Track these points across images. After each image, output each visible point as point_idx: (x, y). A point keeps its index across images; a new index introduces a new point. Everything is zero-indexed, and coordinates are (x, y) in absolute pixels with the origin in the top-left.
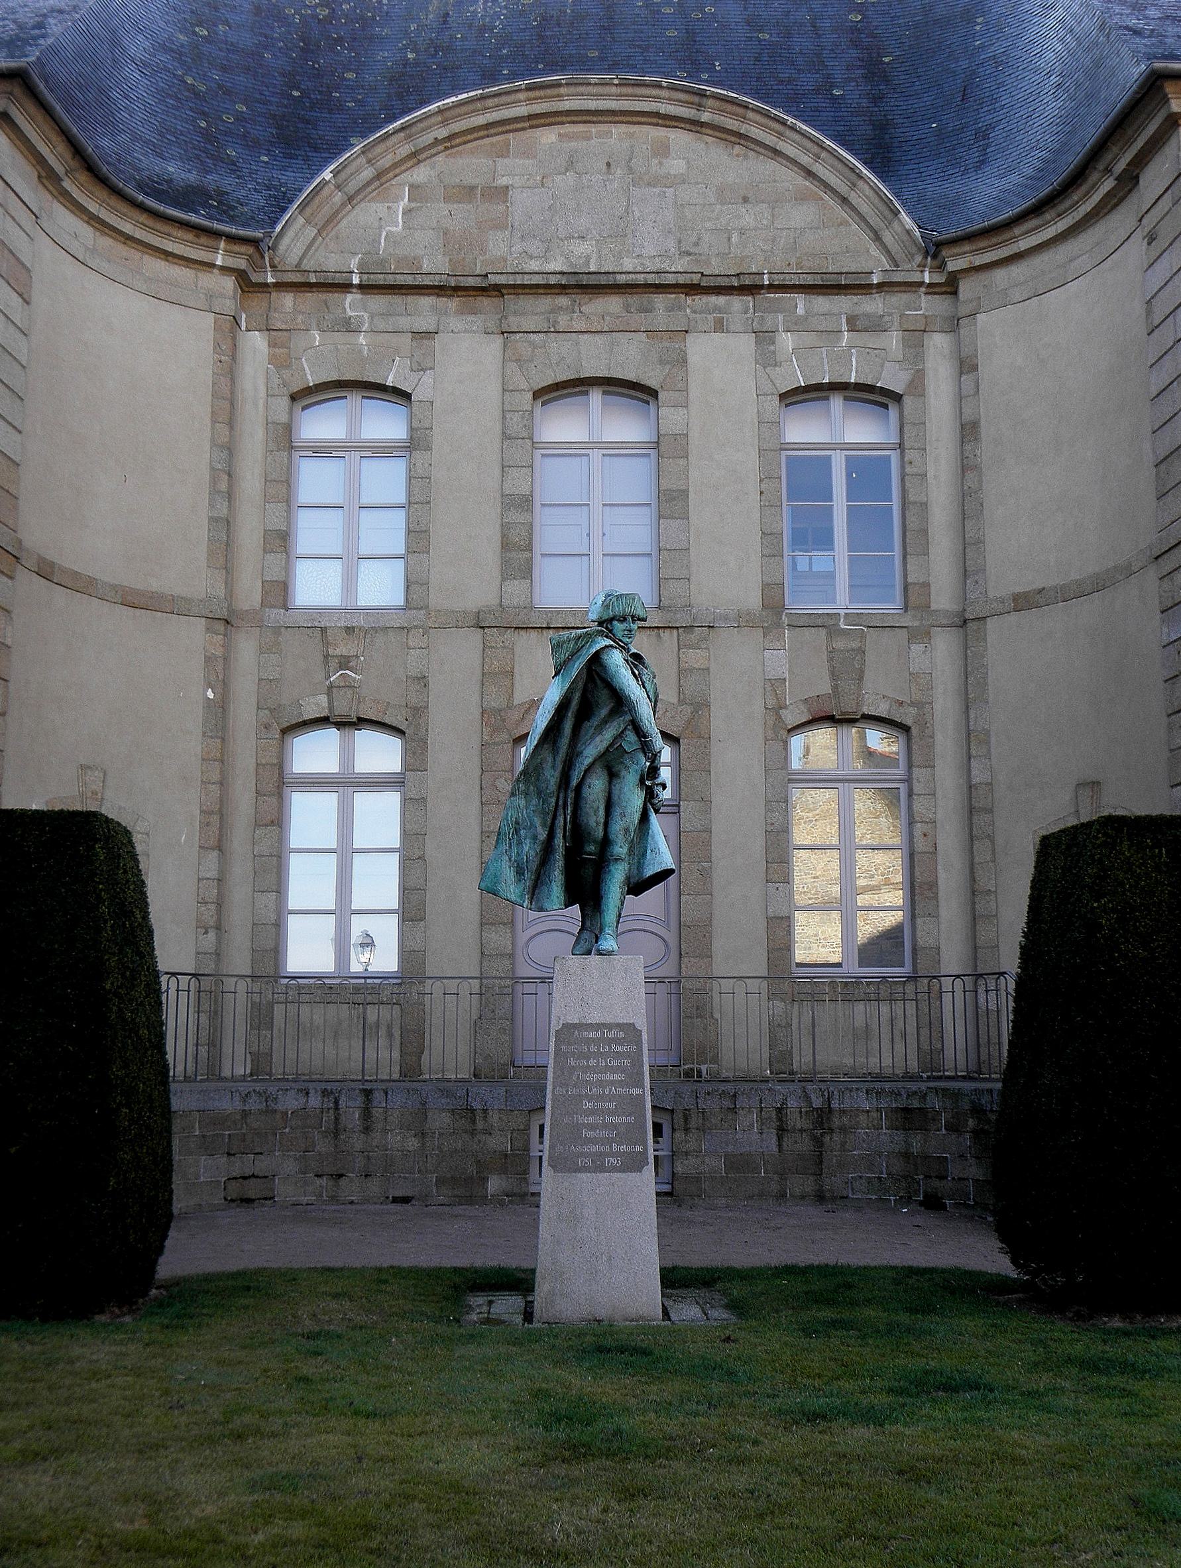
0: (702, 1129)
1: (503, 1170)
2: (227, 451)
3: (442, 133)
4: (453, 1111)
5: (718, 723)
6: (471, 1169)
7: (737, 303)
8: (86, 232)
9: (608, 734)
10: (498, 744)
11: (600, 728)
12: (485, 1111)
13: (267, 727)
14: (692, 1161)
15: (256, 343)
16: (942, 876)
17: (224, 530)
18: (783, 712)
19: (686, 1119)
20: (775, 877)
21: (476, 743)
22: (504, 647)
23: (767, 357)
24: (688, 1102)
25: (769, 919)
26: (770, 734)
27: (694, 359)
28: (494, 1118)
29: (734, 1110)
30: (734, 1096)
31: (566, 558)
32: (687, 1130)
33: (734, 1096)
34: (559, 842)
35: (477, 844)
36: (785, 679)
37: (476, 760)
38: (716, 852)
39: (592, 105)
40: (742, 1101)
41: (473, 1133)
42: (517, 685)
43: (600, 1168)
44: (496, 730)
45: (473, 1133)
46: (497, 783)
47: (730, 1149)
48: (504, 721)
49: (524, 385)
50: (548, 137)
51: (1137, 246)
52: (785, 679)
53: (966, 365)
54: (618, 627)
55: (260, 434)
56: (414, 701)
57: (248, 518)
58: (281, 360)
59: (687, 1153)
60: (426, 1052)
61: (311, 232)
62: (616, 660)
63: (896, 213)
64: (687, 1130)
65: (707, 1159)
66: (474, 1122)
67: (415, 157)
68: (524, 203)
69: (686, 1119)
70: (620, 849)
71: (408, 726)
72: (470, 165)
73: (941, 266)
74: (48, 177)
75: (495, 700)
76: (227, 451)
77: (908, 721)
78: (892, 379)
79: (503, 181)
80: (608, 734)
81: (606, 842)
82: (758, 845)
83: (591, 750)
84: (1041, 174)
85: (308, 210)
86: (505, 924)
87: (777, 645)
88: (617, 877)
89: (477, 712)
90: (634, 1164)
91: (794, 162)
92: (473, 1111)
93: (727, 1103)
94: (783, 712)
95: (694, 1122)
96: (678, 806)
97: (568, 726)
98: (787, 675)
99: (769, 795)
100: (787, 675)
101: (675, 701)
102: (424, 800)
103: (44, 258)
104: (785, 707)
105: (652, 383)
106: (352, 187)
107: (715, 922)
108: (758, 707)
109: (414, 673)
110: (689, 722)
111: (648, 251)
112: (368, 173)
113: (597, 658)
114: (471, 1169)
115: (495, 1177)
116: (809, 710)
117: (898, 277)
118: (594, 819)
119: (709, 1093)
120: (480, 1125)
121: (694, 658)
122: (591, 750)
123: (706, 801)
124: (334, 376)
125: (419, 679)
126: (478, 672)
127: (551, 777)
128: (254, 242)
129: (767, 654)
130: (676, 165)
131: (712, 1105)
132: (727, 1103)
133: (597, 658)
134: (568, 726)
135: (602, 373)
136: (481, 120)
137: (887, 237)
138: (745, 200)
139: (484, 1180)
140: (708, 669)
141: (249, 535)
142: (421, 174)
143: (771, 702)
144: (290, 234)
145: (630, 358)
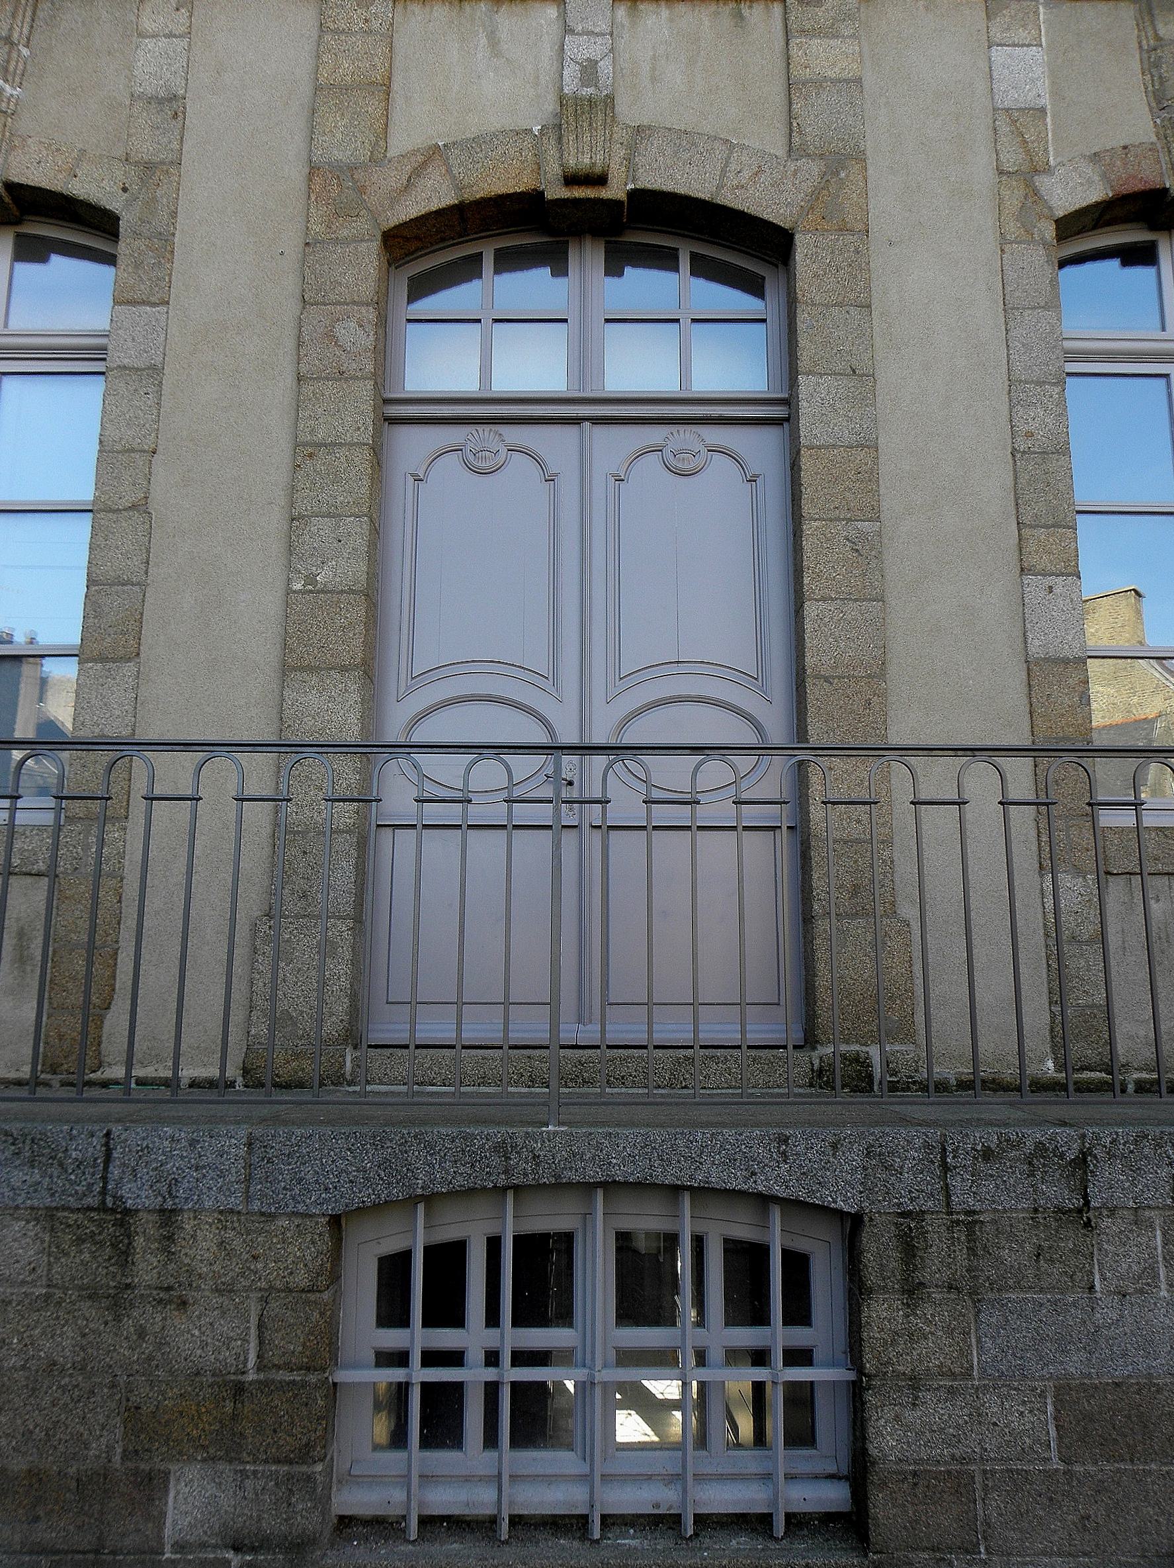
0: (969, 1290)
1: (225, 1446)
4: (49, 1217)
5: (885, 199)
6: (106, 1443)
10: (345, 242)
12: (168, 1216)
14: (935, 1410)
18: (1044, 183)
19: (909, 1248)
20: (1044, 562)
21: (291, 241)
22: (369, 32)
24: (912, 1184)
25: (1029, 664)
26: (1013, 228)
28: (201, 1244)
29: (1082, 1216)
30: (1082, 1161)
31: (578, 674)
32: (912, 1291)
33: (1082, 1161)
35: (280, 476)
36: (1043, 110)
37: (291, 283)
38: (890, 502)
40: (1108, 1184)
41: (117, 1301)
42: (397, 116)
44: (342, 212)
45: (117, 1301)
46: (340, 331)
47: (1074, 1364)
48: (361, 190)
52: (1043, 110)
56: (145, 148)
59: (915, 1382)
60: (121, 1005)
64: (912, 1291)
65: (992, 1405)
66: (124, 1256)
69: (909, 1248)
71: (128, 204)
75: (343, 143)
82: (993, 485)
86: (344, 669)
87: (1022, 35)
89: (296, 173)
92: (124, 1216)
93: (1056, 1192)
94: (1044, 183)
95: (941, 1256)
96: (790, 402)
98: (1046, 101)
99: (1018, 367)
100: (1046, 101)
101: (781, 152)
102: (155, 371)
104: (1048, 170)
107: (892, 670)
108: (980, 169)
109: (150, 87)
110: (815, 195)
114: (106, 1443)
115: (193, 1472)
116: (1104, 176)
119: (987, 1154)
120: (147, 1268)
121: (822, 56)
123: (861, 376)
125: (160, 101)
126: (306, 89)
129: (998, 54)
131: (1000, 1195)
132: (1056, 1192)
139: (151, 1485)
140: (858, 81)
143: (1012, 158)
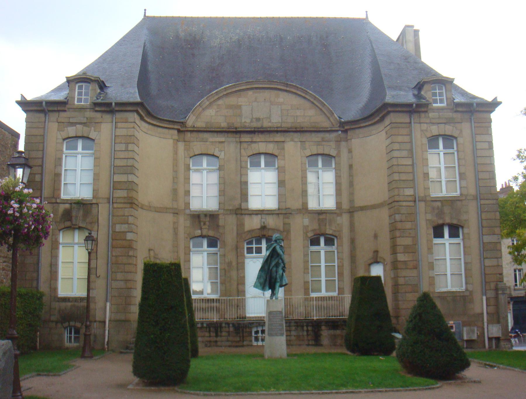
2: (175, 171)
3: (225, 93)
7: (296, 135)
8: (146, 125)
9: (277, 260)
11: (275, 259)
13: (187, 238)
15: (181, 146)
16: (345, 272)
17: (175, 191)
23: (304, 148)
27: (286, 148)
34: (268, 279)
39: (261, 86)
43: (277, 335)
49: (246, 155)
50: (250, 93)
51: (383, 133)
53: (350, 151)
54: (278, 241)
55: (183, 167)
57: (180, 188)
58: (187, 149)
61: (194, 118)
62: (278, 248)
63: (333, 114)
67: (219, 99)
68: (246, 110)
70: (279, 280)
72: (232, 100)
73: (343, 127)
74: (142, 118)
76: (175, 171)
77: (337, 235)
78: (333, 153)
79: (240, 104)
80: (277, 260)
81: (276, 279)
83: (273, 263)
84: (366, 107)
85: (194, 113)
88: (278, 285)
90: (282, 335)
91: (309, 100)
97: (269, 260)
103: (140, 135)
105: (276, 154)
106: (204, 107)
111: (276, 120)
112: (207, 103)
113: (275, 248)
117: (333, 129)
118: (274, 274)
121: (287, 221)
122: (273, 263)
124: (200, 153)
127: (266, 267)
128: (182, 123)
130: (281, 100)
133: (275, 248)
134: (269, 260)
135: (264, 152)
136: (234, 90)
137: (331, 119)
138: (298, 109)
141: (181, 192)
142: (220, 102)
144: (190, 118)
145: (271, 148)
